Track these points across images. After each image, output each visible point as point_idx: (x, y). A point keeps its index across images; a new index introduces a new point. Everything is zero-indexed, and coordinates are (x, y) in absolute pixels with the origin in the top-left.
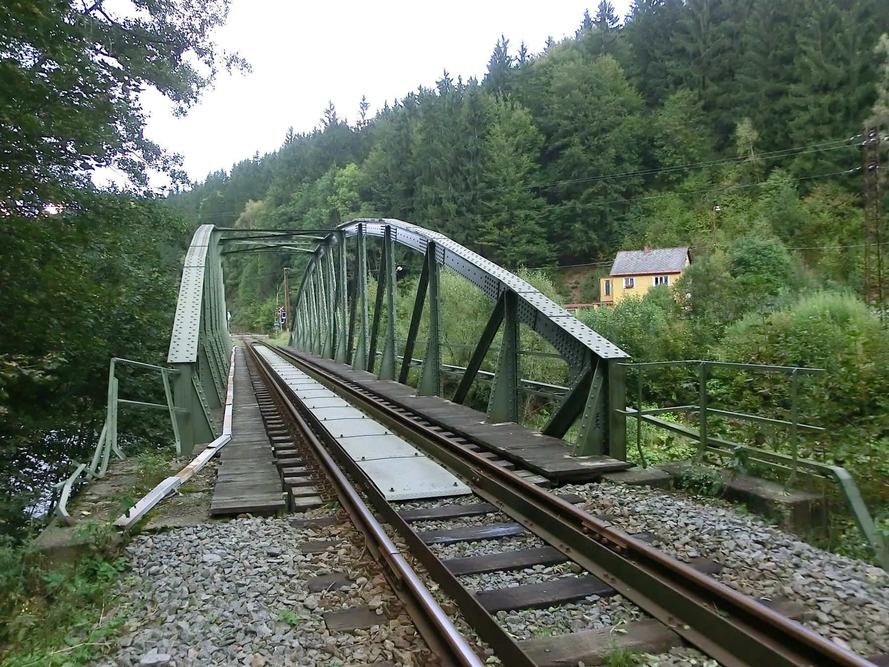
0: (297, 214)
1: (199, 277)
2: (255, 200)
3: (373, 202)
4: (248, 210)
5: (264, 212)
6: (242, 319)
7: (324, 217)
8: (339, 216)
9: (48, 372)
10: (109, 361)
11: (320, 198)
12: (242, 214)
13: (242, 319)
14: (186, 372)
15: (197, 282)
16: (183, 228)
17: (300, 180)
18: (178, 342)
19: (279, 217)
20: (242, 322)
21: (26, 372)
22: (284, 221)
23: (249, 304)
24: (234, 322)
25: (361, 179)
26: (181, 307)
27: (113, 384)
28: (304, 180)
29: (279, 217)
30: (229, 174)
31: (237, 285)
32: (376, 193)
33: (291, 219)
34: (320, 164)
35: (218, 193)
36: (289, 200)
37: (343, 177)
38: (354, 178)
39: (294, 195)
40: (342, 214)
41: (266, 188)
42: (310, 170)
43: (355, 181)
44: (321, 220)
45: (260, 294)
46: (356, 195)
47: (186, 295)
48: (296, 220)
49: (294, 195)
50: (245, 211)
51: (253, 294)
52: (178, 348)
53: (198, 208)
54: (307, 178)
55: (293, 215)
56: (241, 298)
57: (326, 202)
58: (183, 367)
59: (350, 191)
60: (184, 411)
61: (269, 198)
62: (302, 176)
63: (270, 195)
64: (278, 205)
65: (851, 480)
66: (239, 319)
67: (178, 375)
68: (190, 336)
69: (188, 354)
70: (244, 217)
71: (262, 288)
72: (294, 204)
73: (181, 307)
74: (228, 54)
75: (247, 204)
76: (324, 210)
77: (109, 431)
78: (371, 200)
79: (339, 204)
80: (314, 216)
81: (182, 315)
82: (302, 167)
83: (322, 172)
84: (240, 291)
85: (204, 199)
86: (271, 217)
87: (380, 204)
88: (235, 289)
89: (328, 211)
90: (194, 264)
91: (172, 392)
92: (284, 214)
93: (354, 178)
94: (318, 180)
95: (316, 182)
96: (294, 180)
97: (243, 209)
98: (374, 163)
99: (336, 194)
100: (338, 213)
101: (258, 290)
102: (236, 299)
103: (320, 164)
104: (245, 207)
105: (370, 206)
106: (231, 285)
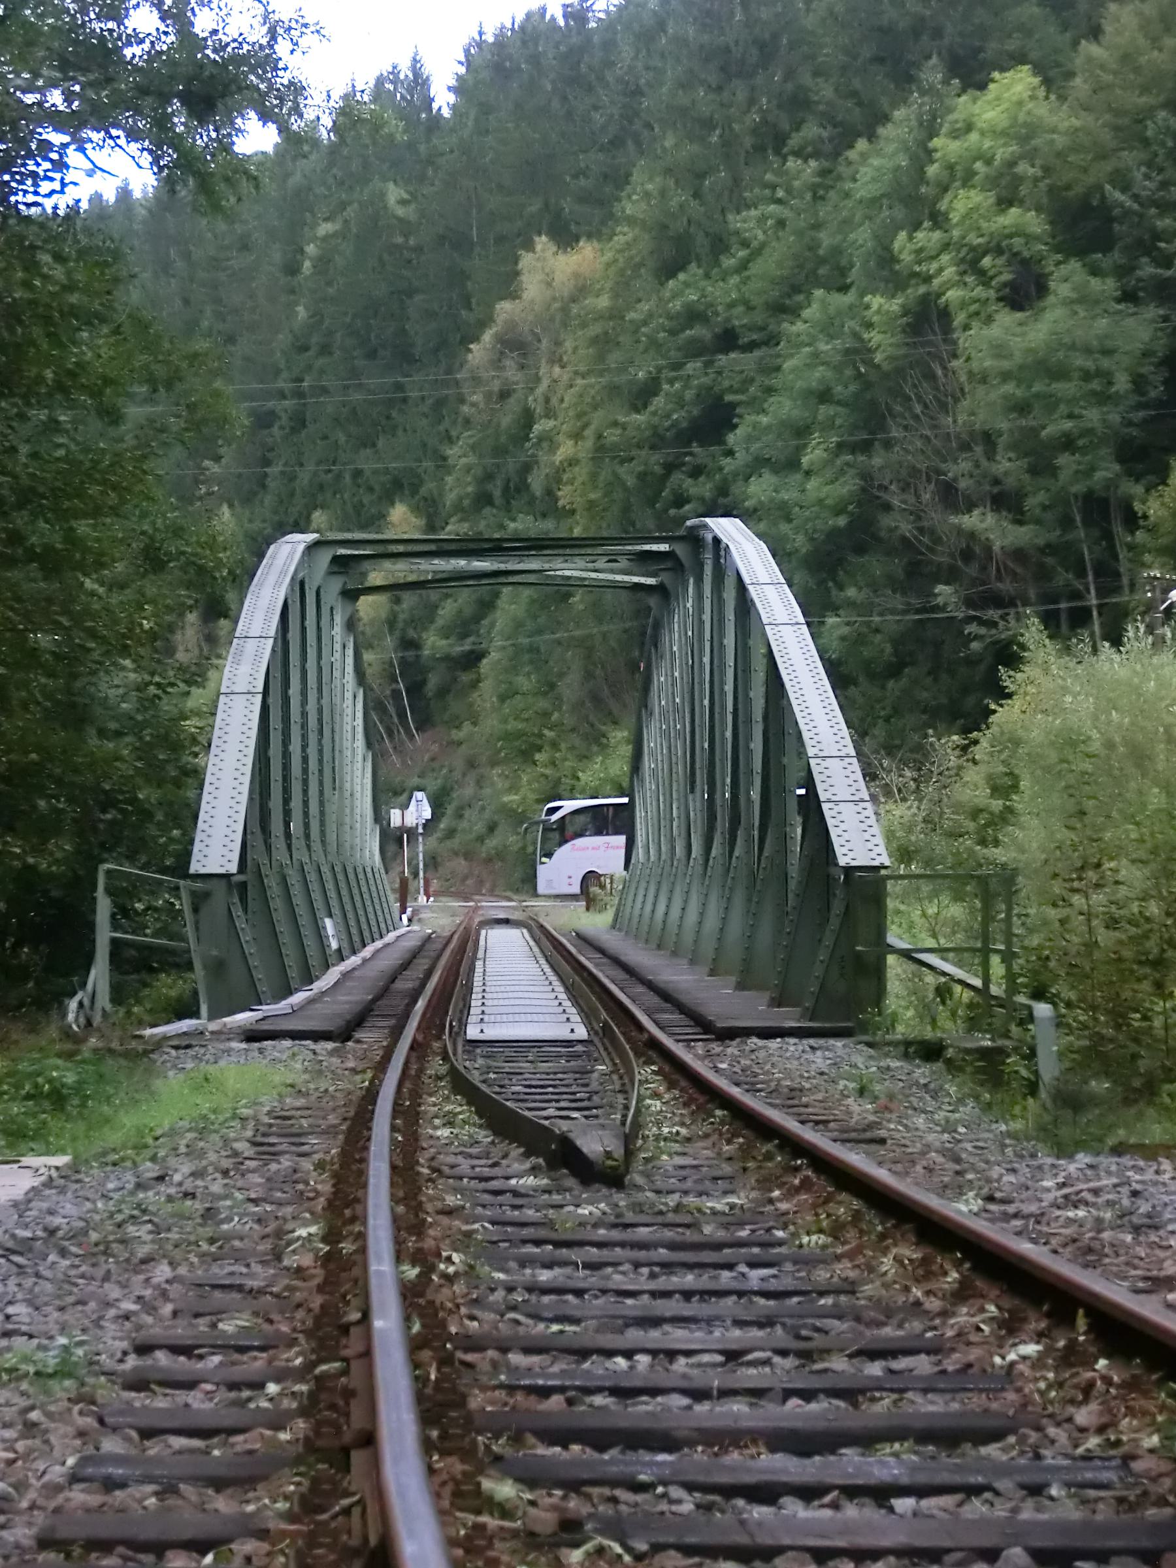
0: (759, 318)
1: (250, 716)
2: (565, 238)
3: (1117, 256)
4: (532, 287)
5: (604, 302)
6: (492, 828)
7: (874, 337)
8: (947, 329)
9: (57, 862)
10: (96, 869)
11: (863, 236)
12: (505, 309)
13: (492, 828)
14: (219, 888)
15: (245, 729)
16: (220, 564)
17: (779, 141)
18: (207, 841)
19: (673, 333)
20: (492, 843)
21: (31, 860)
22: (695, 350)
23: (527, 755)
24: (455, 843)
25: (1060, 141)
26: (207, 818)
27: (104, 907)
28: (794, 141)
29: (673, 333)
30: (443, 100)
31: (473, 659)
32: (1128, 213)
33: (728, 340)
34: (879, 60)
35: (394, 193)
36: (719, 245)
37: (974, 137)
38: (1024, 140)
39: (744, 222)
40: (959, 319)
41: (619, 179)
42: (826, 91)
43: (1030, 156)
44: (859, 352)
45: (578, 705)
46: (1034, 222)
47: (222, 755)
48: (751, 346)
49: (744, 222)
50: (514, 296)
51: (543, 704)
52: (206, 851)
53: (292, 269)
54: (812, 130)
55: (739, 318)
56: (491, 724)
57: (887, 258)
58: (215, 881)
59: (1005, 203)
60: (215, 953)
61: (624, 235)
62: (786, 126)
63: (631, 221)
64: (669, 270)
65: (1050, 1019)
66: (480, 828)
67: (207, 895)
68: (228, 831)
69: (224, 861)
70: (511, 325)
71: (589, 675)
72: (744, 265)
73: (207, 818)
74: (335, 96)
75: (526, 260)
76: (876, 301)
77: (99, 975)
78: (1107, 249)
79: (950, 272)
80: (829, 328)
81: (213, 812)
82: (789, 75)
83: (884, 102)
84: (486, 695)
85: (325, 228)
86: (637, 326)
87: (1147, 270)
88: (465, 678)
89: (895, 305)
90: (255, 632)
91: (197, 929)
92: (693, 316)
93: (1024, 140)
94: (862, 144)
95: (852, 154)
96: (748, 142)
97: (509, 285)
98: (1126, 58)
99: (938, 220)
100: (945, 315)
101: (571, 687)
102: (467, 727)
103: (879, 60)
104: (517, 273)
105: (1095, 283)
106: (447, 658)
